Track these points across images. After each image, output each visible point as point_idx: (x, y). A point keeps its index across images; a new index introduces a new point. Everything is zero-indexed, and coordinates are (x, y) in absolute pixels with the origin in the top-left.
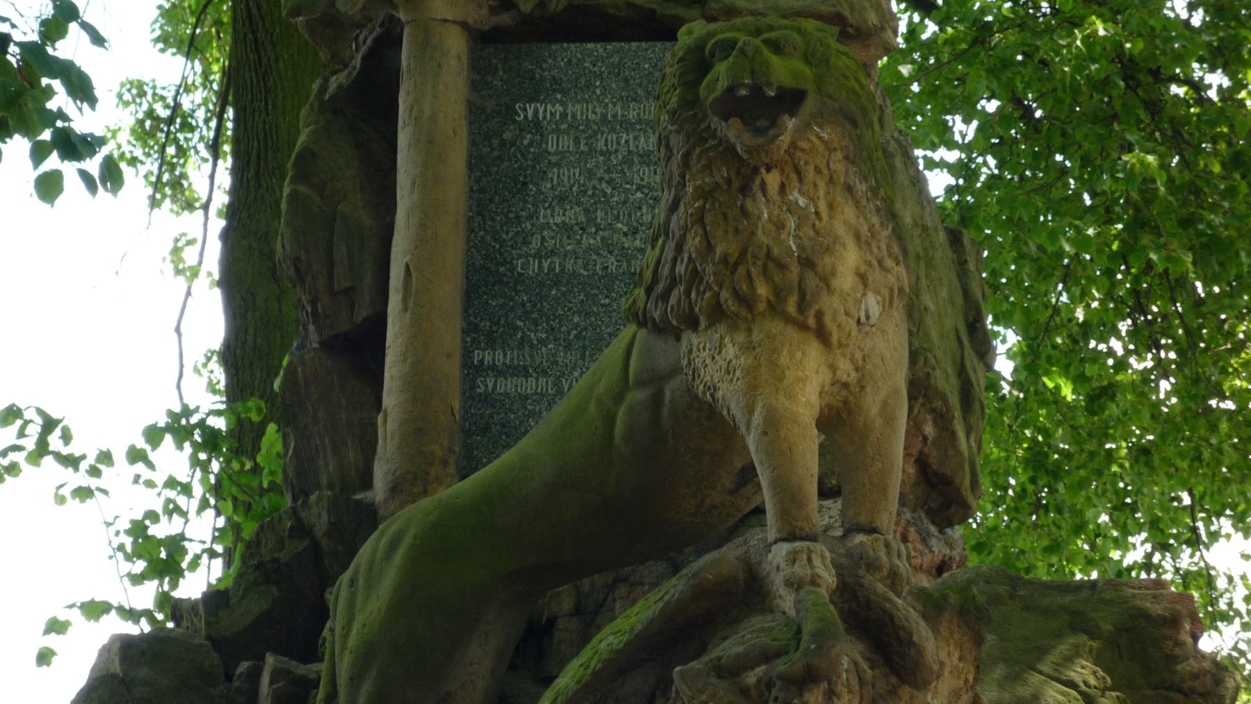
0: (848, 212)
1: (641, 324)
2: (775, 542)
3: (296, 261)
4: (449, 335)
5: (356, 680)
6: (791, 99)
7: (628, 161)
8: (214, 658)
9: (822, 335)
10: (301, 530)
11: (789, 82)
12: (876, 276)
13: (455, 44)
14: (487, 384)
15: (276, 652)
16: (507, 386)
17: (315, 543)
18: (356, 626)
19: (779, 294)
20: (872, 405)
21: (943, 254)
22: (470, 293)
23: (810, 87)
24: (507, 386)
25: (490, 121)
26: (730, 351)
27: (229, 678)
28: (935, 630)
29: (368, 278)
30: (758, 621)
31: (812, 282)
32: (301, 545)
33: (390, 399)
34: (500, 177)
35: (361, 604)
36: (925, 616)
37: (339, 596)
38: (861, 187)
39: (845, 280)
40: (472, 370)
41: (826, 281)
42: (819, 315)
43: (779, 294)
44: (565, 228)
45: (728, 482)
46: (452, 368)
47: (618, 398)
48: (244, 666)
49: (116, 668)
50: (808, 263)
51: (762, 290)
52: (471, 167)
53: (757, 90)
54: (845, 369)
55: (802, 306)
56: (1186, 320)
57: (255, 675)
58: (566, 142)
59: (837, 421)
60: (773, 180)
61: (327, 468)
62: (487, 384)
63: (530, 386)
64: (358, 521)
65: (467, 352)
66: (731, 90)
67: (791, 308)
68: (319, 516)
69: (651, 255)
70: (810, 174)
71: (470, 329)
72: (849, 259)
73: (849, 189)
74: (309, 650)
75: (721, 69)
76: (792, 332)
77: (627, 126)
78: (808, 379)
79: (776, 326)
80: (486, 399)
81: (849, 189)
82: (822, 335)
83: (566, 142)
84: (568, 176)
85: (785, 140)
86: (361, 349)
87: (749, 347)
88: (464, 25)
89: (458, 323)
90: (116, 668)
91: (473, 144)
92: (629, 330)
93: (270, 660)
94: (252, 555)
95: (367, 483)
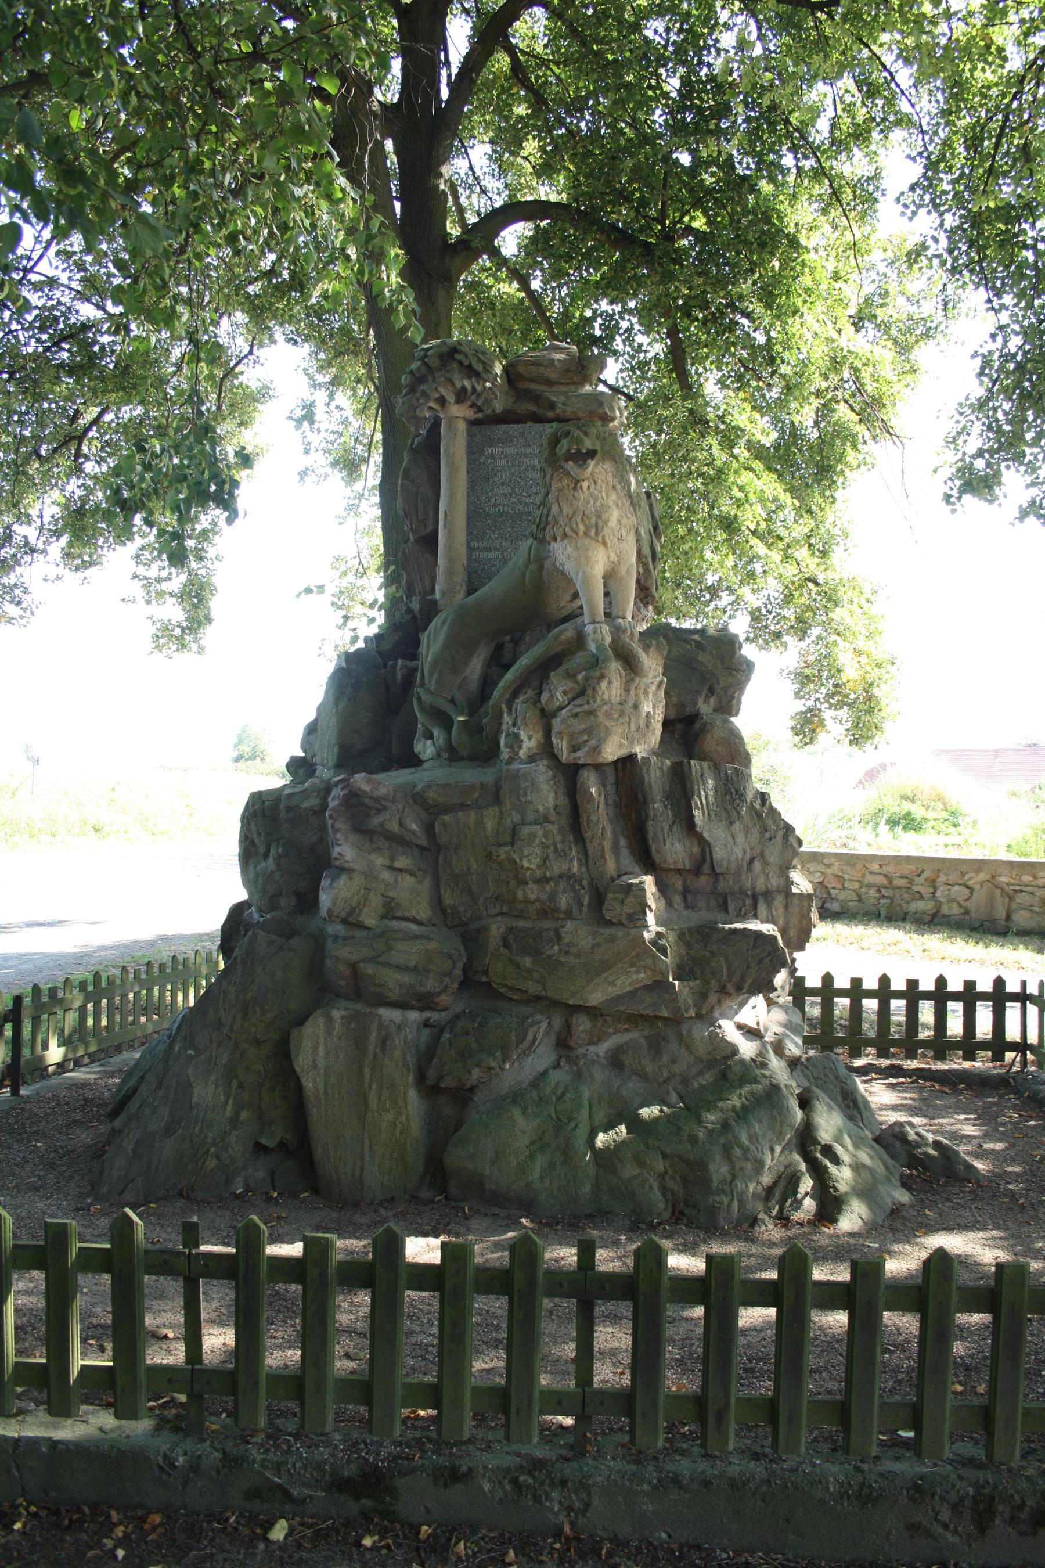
0: (614, 497)
1: (535, 538)
2: (780, 1006)
3: (404, 510)
4: (461, 537)
5: (431, 673)
6: (592, 454)
7: (526, 469)
8: (380, 660)
9: (604, 544)
10: (409, 611)
11: (591, 447)
12: (624, 520)
13: (462, 426)
14: (476, 554)
15: (403, 658)
16: (484, 555)
17: (415, 617)
18: (432, 650)
19: (588, 529)
20: (623, 569)
21: (644, 503)
22: (469, 520)
23: (599, 449)
24: (484, 555)
25: (473, 450)
26: (569, 550)
27: (385, 666)
28: (647, 654)
29: (431, 515)
30: (581, 653)
31: (600, 524)
32: (410, 616)
33: (440, 561)
34: (479, 478)
35: (433, 643)
36: (643, 649)
37: (424, 637)
38: (618, 487)
39: (613, 522)
40: (471, 549)
41: (606, 522)
42: (603, 537)
43: (588, 529)
44: (505, 495)
45: (568, 597)
46: (463, 550)
47: (527, 567)
48: (390, 663)
49: (344, 665)
50: (599, 517)
51: (582, 528)
52: (468, 472)
53: (579, 451)
54: (613, 556)
55: (597, 534)
56: (127, 144)
57: (394, 667)
58: (504, 462)
59: (609, 577)
60: (585, 484)
61: (418, 587)
62: (476, 554)
63: (492, 555)
64: (431, 609)
65: (468, 543)
66: (569, 450)
67: (593, 533)
68: (415, 605)
69: (538, 513)
70: (599, 482)
71: (469, 533)
72: (614, 515)
73: (614, 487)
74: (414, 657)
75: (564, 442)
76: (593, 543)
77: (526, 456)
78: (599, 562)
79: (587, 541)
80: (476, 560)
81: (614, 487)
82: (604, 544)
83: (504, 462)
84: (505, 475)
85: (590, 469)
86: (430, 542)
87: (577, 549)
88: (464, 418)
89: (465, 532)
90: (344, 665)
91: (469, 464)
92: (530, 540)
93: (400, 662)
94: (393, 625)
95: (433, 591)
